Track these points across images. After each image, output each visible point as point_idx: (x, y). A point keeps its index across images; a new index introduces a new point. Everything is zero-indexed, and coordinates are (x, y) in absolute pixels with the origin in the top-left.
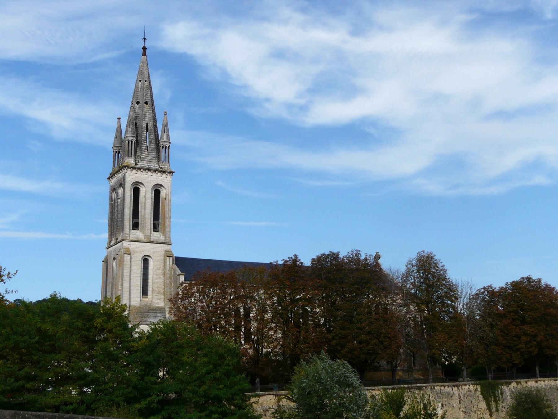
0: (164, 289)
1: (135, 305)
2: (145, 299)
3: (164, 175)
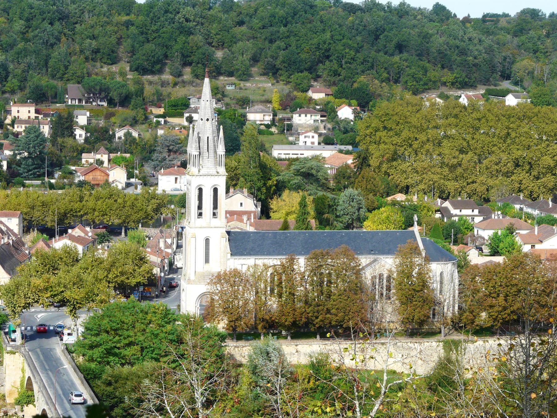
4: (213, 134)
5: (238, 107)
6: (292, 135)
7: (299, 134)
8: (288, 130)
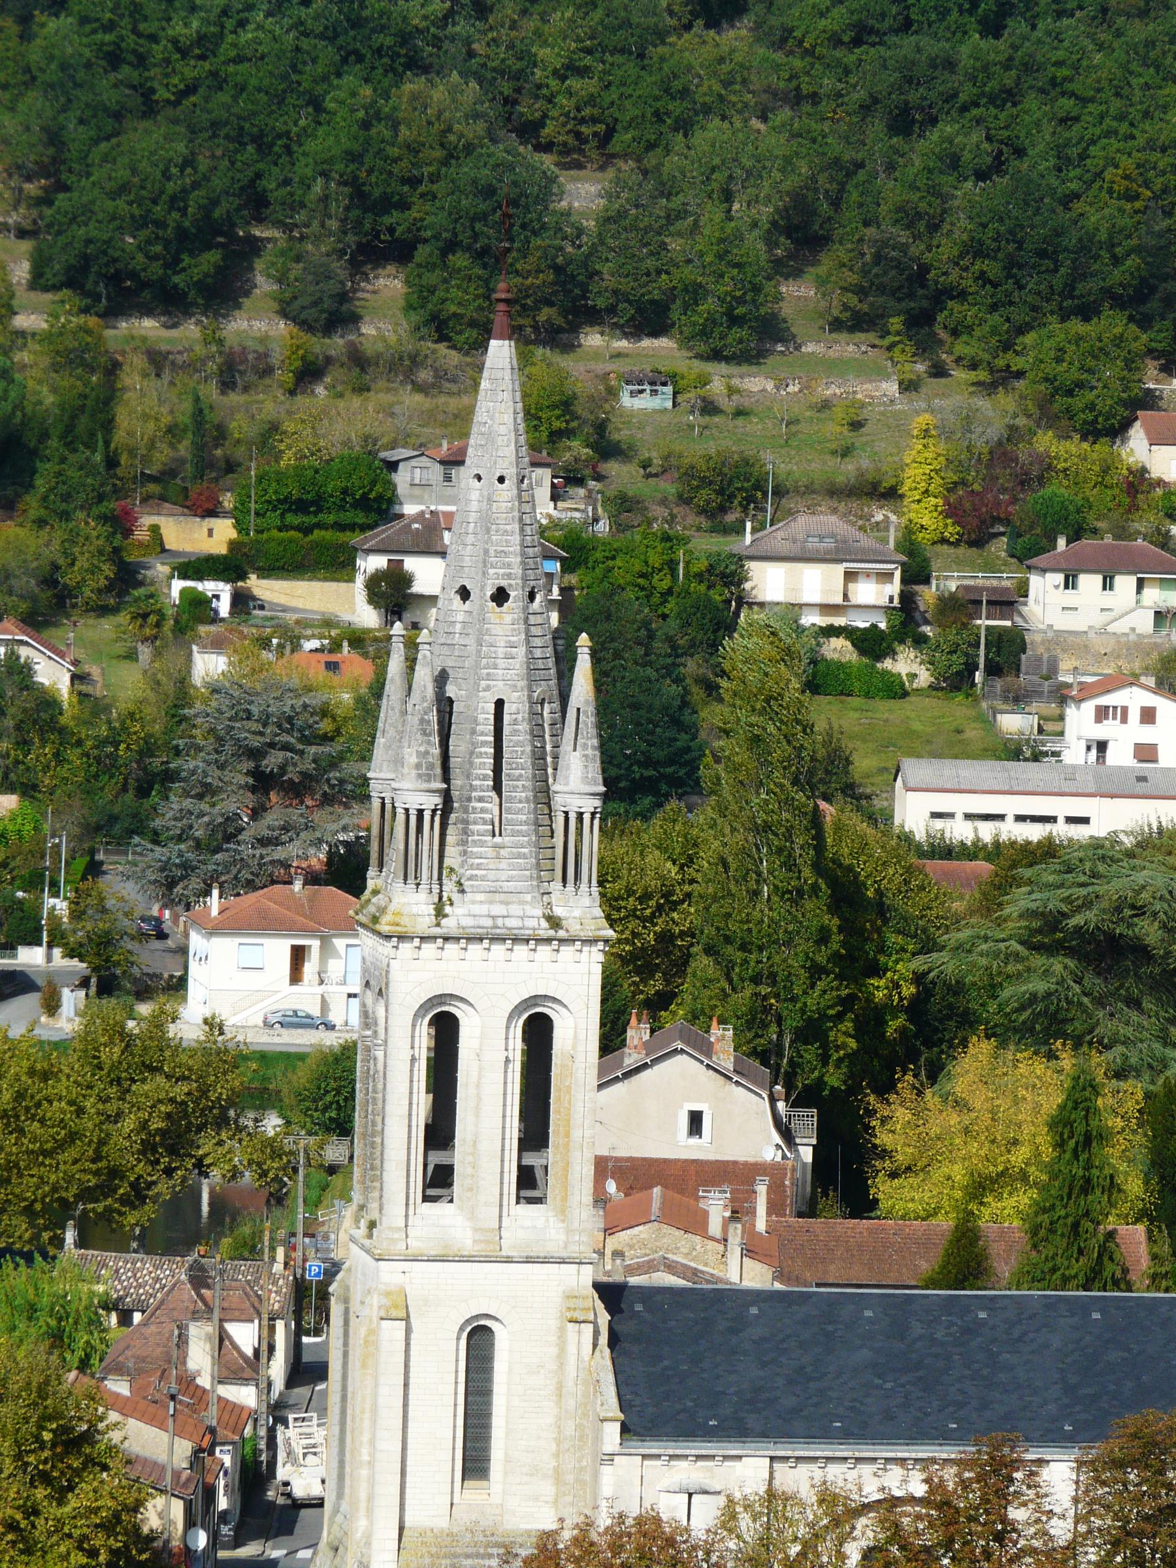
0: (557, 1455)
1: (428, 1523)
2: (473, 1495)
3: (567, 951)
4: (531, 682)
5: (688, 521)
6: (1018, 700)
7: (1062, 696)
8: (993, 670)
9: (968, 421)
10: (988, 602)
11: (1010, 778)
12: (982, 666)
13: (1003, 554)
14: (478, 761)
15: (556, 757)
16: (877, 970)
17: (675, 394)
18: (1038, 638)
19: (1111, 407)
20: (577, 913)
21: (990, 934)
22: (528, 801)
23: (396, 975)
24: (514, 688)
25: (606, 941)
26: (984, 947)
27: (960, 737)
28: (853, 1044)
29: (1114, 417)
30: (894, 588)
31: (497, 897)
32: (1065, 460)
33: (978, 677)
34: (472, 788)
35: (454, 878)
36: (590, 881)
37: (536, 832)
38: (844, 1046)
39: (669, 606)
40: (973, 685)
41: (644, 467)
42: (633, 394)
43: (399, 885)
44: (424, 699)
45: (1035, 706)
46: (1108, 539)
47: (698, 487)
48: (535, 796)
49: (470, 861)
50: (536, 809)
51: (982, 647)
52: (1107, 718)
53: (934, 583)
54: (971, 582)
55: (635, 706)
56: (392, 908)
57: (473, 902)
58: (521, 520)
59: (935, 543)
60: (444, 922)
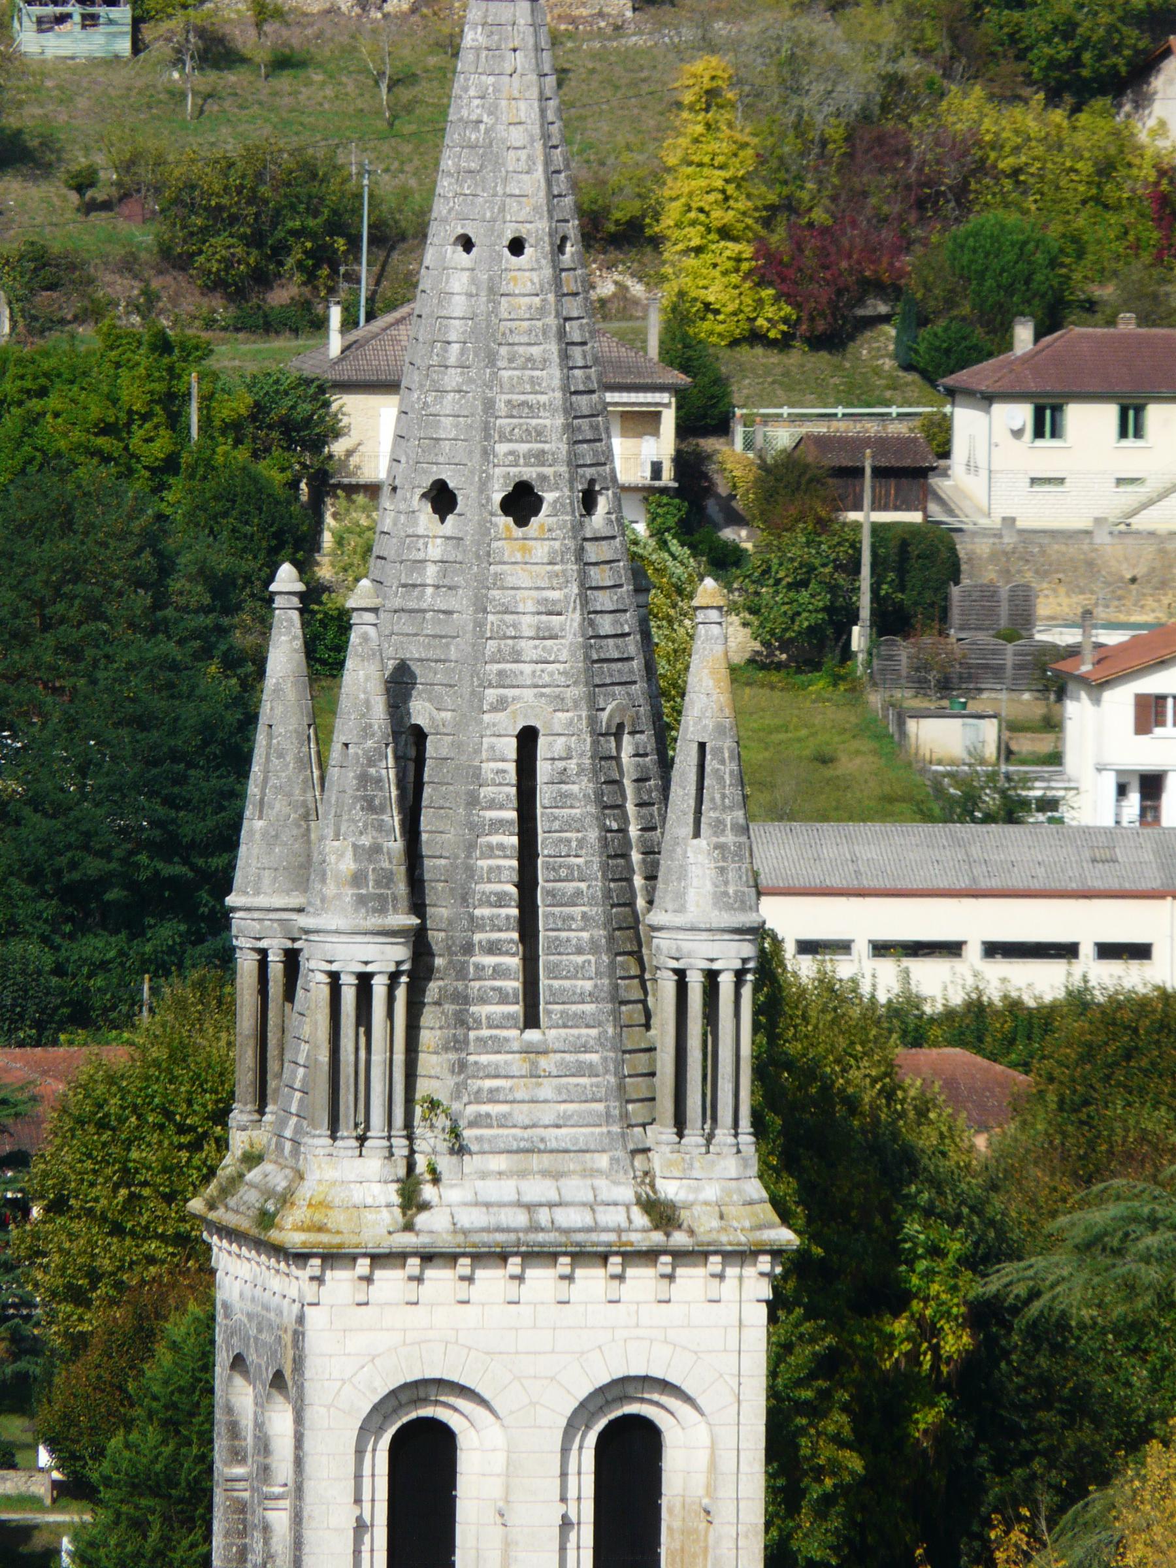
3: (692, 1278)
4: (595, 688)
5: (185, 306)
6: (950, 687)
7: (1054, 676)
8: (891, 622)
9: (793, 66)
10: (878, 472)
11: (970, 862)
12: (865, 613)
13: (888, 364)
14: (484, 864)
15: (651, 852)
16: (899, 1301)
17: (137, 22)
18: (983, 548)
19: (1111, 29)
20: (711, 1192)
21: (1161, 1212)
22: (594, 948)
23: (318, 1339)
24: (559, 704)
25: (776, 1254)
26: (1152, 1241)
27: (828, 772)
28: (855, 1463)
29: (1117, 49)
30: (662, 445)
31: (535, 1161)
32: (1016, 150)
33: (858, 637)
34: (475, 925)
35: (442, 1121)
36: (736, 1125)
37: (616, 1015)
38: (834, 1467)
39: (170, 497)
40: (847, 654)
41: (80, 189)
42: (44, 26)
43: (318, 1142)
44: (366, 732)
45: (985, 701)
46: (1127, 324)
47: (204, 230)
48: (611, 939)
49: (473, 1084)
50: (612, 965)
51: (866, 571)
52: (1161, 723)
53: (739, 431)
54: (820, 428)
55: (141, 723)
56: (307, 1190)
57: (484, 1175)
58: (562, 334)
59: (734, 343)
60: (422, 1220)
